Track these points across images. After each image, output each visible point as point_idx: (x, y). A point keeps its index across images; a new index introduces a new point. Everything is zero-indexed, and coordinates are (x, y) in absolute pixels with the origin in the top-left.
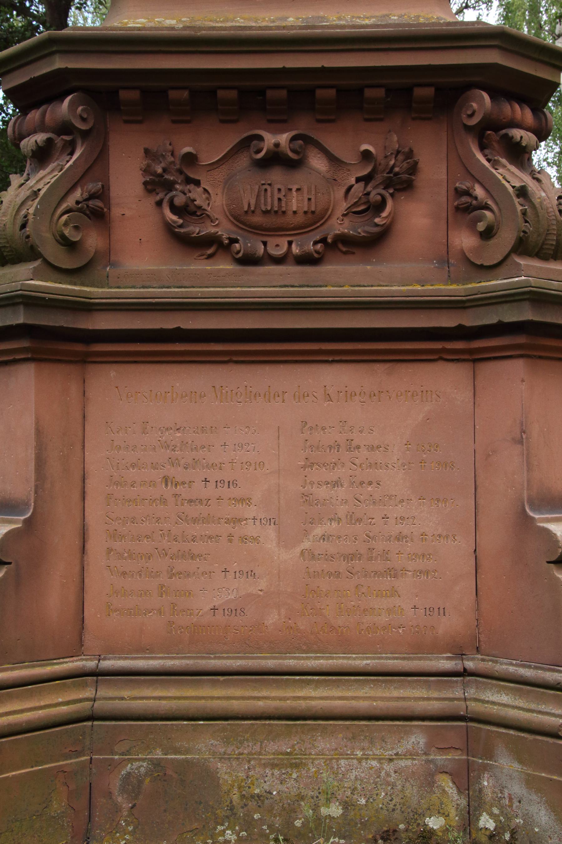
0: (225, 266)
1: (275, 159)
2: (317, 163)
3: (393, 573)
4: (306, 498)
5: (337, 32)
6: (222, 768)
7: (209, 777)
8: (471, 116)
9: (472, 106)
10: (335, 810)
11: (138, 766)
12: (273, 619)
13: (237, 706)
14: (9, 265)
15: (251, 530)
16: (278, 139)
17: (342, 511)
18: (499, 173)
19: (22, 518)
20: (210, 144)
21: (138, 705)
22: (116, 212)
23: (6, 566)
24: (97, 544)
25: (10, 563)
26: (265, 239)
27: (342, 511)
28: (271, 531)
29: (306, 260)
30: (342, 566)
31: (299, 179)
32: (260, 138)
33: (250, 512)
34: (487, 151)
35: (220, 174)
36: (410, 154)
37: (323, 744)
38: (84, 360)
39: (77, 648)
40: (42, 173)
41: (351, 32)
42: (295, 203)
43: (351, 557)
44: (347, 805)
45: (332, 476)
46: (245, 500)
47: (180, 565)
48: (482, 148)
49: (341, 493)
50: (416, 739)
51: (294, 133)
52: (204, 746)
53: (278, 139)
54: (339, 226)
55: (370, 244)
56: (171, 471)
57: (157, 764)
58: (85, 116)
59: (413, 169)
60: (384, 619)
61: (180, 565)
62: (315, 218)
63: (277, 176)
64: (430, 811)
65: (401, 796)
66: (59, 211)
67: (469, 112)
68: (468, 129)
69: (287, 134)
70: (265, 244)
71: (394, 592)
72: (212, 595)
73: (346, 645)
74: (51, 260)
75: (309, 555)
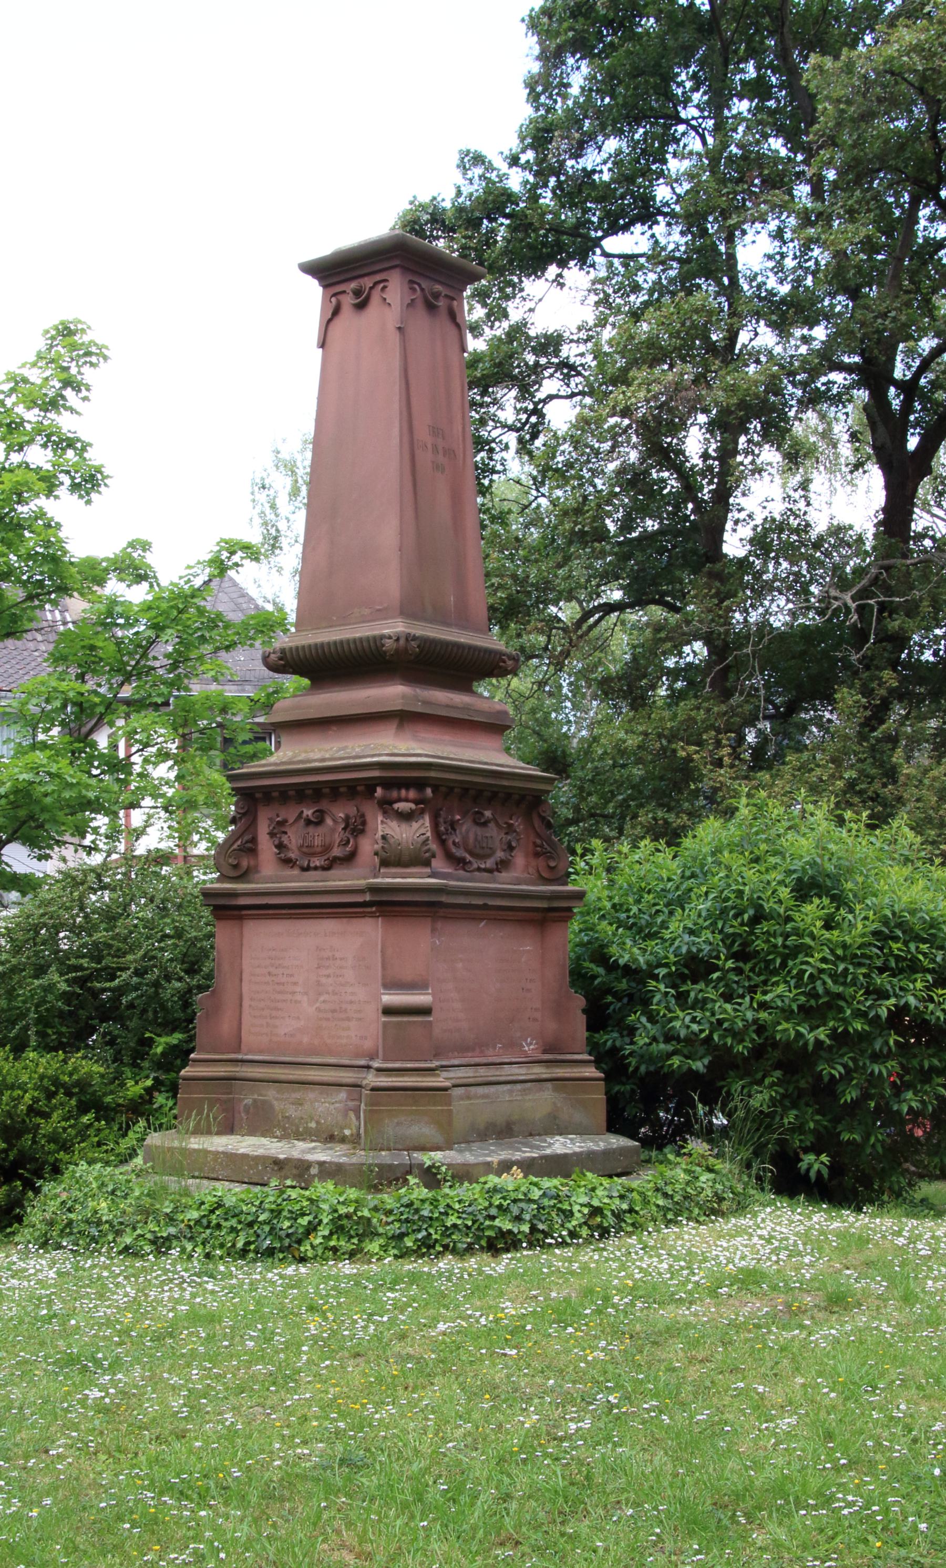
0: (296, 872)
2: (329, 822)
3: (348, 1019)
4: (319, 983)
6: (275, 1103)
7: (271, 1107)
10: (313, 1125)
11: (248, 1101)
12: (306, 1040)
13: (283, 1077)
15: (298, 997)
17: (330, 989)
20: (289, 813)
21: (249, 1075)
22: (260, 847)
24: (246, 1003)
27: (330, 989)
28: (305, 998)
29: (490, 871)
30: (330, 1015)
31: (321, 830)
33: (298, 989)
35: (294, 829)
36: (363, 816)
37: (311, 1094)
38: (241, 918)
39: (238, 1050)
42: (317, 842)
43: (334, 1011)
44: (318, 1123)
45: (326, 972)
46: (295, 984)
47: (274, 1013)
49: (330, 980)
50: (343, 1095)
52: (270, 1093)
53: (308, 812)
54: (337, 852)
55: (350, 858)
56: (272, 970)
57: (255, 1101)
59: (364, 823)
60: (344, 1041)
61: (274, 1013)
62: (327, 848)
63: (311, 829)
64: (346, 1127)
65: (898, 1430)
71: (348, 1029)
72: (286, 1027)
73: (331, 1053)
75: (318, 1010)
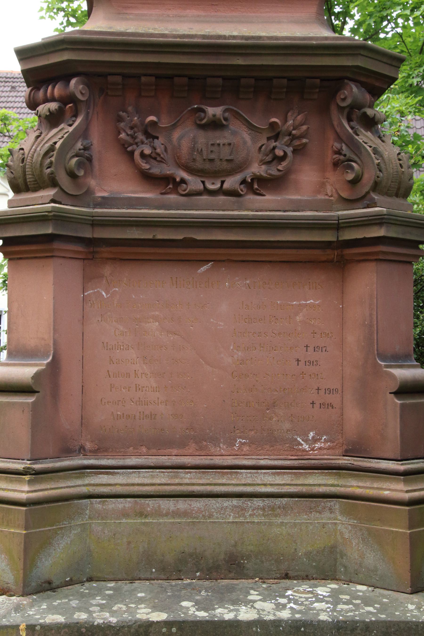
1: (215, 125)
5: (185, 42)
8: (344, 100)
9: (344, 93)
14: (23, 193)
16: (214, 111)
18: (360, 139)
19: (45, 362)
23: (37, 394)
25: (38, 392)
26: (203, 180)
32: (203, 111)
34: (352, 123)
40: (55, 131)
41: (172, 41)
48: (349, 120)
51: (226, 107)
54: (257, 169)
58: (84, 92)
66: (69, 156)
67: (342, 97)
68: (341, 109)
69: (222, 107)
70: (203, 182)
74: (64, 187)
